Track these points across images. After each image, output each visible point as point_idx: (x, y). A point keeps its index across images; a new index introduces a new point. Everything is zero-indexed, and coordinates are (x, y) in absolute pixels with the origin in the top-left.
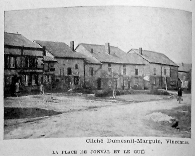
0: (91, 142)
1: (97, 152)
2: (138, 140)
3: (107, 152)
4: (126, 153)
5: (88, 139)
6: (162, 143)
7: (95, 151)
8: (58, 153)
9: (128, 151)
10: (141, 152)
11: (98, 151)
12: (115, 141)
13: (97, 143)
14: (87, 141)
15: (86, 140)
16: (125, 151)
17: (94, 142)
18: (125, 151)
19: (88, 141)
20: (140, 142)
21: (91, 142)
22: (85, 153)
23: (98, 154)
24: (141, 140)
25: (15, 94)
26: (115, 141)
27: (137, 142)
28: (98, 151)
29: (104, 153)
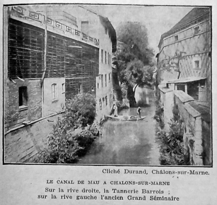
0: (107, 173)
1: (128, 183)
2: (191, 171)
3: (71, 182)
4: (49, 183)
5: (104, 169)
6: (147, 174)
7: (127, 182)
8: (106, 183)
9: (51, 181)
10: (145, 183)
11: (163, 182)
12: (133, 172)
13: (113, 174)
14: (104, 172)
15: (102, 170)
16: (48, 181)
17: (110, 172)
18: (48, 181)
19: (104, 171)
20: (193, 173)
21: (107, 173)
22: (82, 183)
23: (129, 185)
24: (194, 171)
25: (124, 78)
26: (133, 172)
27: (190, 173)
28: (129, 182)
29: (61, 183)
